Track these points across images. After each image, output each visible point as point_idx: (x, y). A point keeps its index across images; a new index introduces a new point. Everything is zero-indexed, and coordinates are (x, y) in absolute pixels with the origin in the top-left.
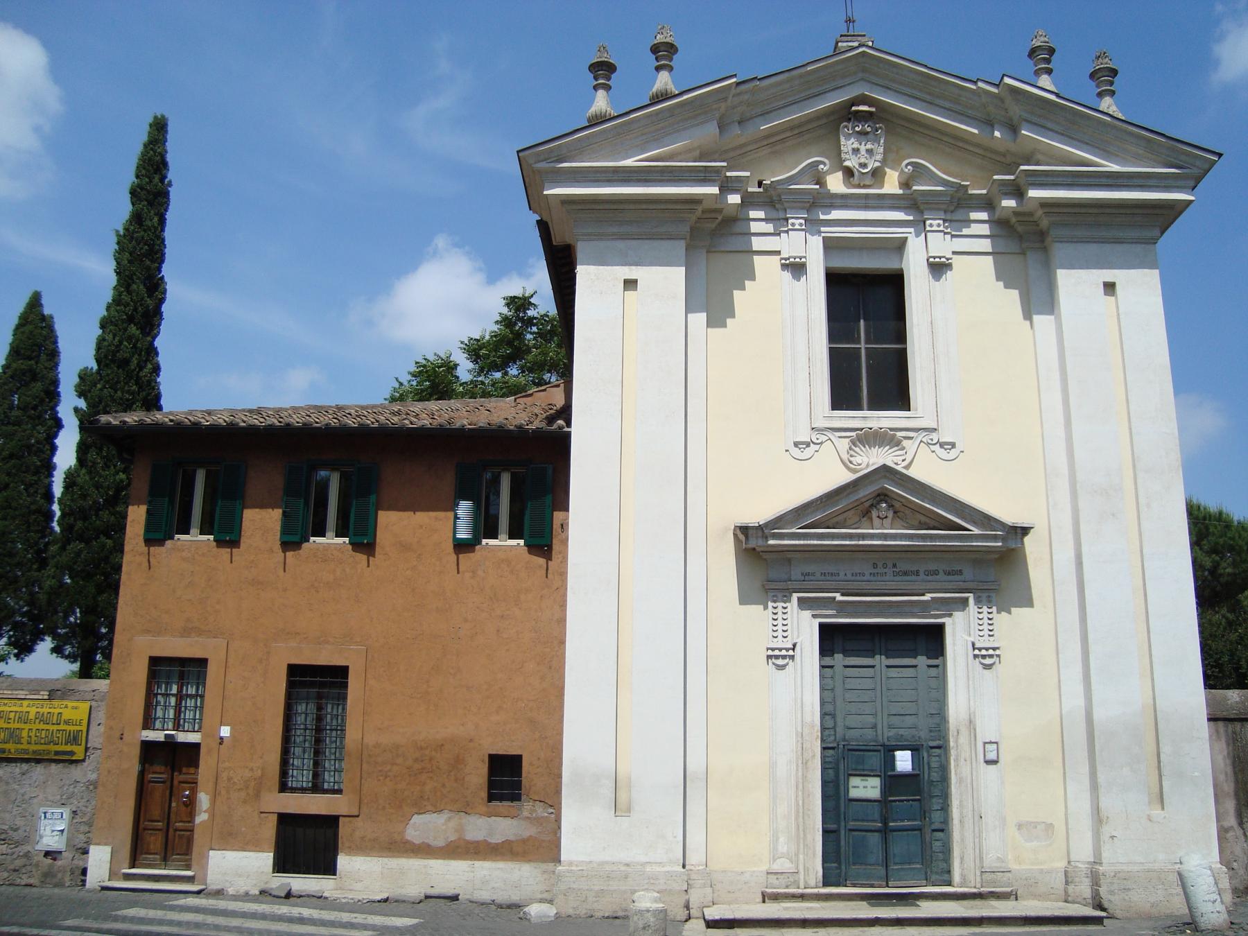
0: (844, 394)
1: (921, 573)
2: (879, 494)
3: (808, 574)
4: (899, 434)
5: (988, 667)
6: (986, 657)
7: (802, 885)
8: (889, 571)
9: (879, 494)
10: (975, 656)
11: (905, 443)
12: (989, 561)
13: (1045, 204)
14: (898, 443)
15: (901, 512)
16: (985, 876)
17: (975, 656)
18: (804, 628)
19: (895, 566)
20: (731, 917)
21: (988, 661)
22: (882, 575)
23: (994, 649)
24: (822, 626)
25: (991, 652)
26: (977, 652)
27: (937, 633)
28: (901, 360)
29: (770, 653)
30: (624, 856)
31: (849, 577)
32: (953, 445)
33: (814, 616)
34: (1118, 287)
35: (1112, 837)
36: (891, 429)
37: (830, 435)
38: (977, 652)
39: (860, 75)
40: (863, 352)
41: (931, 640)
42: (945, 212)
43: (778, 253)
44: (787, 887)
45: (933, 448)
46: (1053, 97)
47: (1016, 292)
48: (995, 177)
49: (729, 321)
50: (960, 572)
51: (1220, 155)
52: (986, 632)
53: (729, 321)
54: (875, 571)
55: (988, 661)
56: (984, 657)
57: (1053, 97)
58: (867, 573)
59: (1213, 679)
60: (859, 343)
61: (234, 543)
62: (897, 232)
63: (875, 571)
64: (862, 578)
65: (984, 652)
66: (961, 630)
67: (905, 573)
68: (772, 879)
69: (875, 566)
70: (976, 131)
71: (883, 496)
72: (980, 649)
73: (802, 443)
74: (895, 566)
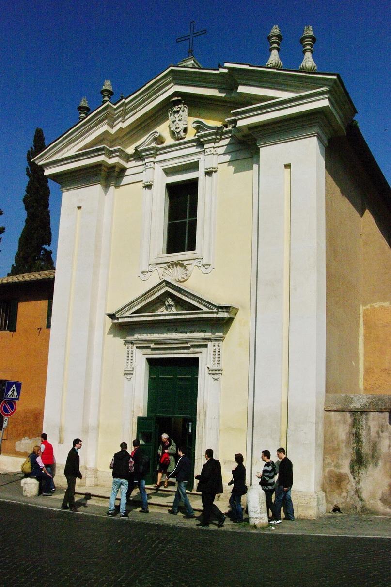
2: (171, 295)
4: (185, 263)
6: (215, 373)
9: (171, 295)
25: (217, 372)
26: (211, 372)
36: (181, 261)
37: (155, 266)
38: (211, 372)
40: (185, 220)
43: (142, 181)
45: (200, 268)
46: (275, 71)
47: (63, 194)
48: (226, 120)
52: (216, 362)
55: (216, 377)
56: (213, 374)
57: (275, 71)
60: (186, 218)
61: (14, 331)
65: (214, 372)
66: (206, 359)
72: (212, 371)
73: (145, 272)
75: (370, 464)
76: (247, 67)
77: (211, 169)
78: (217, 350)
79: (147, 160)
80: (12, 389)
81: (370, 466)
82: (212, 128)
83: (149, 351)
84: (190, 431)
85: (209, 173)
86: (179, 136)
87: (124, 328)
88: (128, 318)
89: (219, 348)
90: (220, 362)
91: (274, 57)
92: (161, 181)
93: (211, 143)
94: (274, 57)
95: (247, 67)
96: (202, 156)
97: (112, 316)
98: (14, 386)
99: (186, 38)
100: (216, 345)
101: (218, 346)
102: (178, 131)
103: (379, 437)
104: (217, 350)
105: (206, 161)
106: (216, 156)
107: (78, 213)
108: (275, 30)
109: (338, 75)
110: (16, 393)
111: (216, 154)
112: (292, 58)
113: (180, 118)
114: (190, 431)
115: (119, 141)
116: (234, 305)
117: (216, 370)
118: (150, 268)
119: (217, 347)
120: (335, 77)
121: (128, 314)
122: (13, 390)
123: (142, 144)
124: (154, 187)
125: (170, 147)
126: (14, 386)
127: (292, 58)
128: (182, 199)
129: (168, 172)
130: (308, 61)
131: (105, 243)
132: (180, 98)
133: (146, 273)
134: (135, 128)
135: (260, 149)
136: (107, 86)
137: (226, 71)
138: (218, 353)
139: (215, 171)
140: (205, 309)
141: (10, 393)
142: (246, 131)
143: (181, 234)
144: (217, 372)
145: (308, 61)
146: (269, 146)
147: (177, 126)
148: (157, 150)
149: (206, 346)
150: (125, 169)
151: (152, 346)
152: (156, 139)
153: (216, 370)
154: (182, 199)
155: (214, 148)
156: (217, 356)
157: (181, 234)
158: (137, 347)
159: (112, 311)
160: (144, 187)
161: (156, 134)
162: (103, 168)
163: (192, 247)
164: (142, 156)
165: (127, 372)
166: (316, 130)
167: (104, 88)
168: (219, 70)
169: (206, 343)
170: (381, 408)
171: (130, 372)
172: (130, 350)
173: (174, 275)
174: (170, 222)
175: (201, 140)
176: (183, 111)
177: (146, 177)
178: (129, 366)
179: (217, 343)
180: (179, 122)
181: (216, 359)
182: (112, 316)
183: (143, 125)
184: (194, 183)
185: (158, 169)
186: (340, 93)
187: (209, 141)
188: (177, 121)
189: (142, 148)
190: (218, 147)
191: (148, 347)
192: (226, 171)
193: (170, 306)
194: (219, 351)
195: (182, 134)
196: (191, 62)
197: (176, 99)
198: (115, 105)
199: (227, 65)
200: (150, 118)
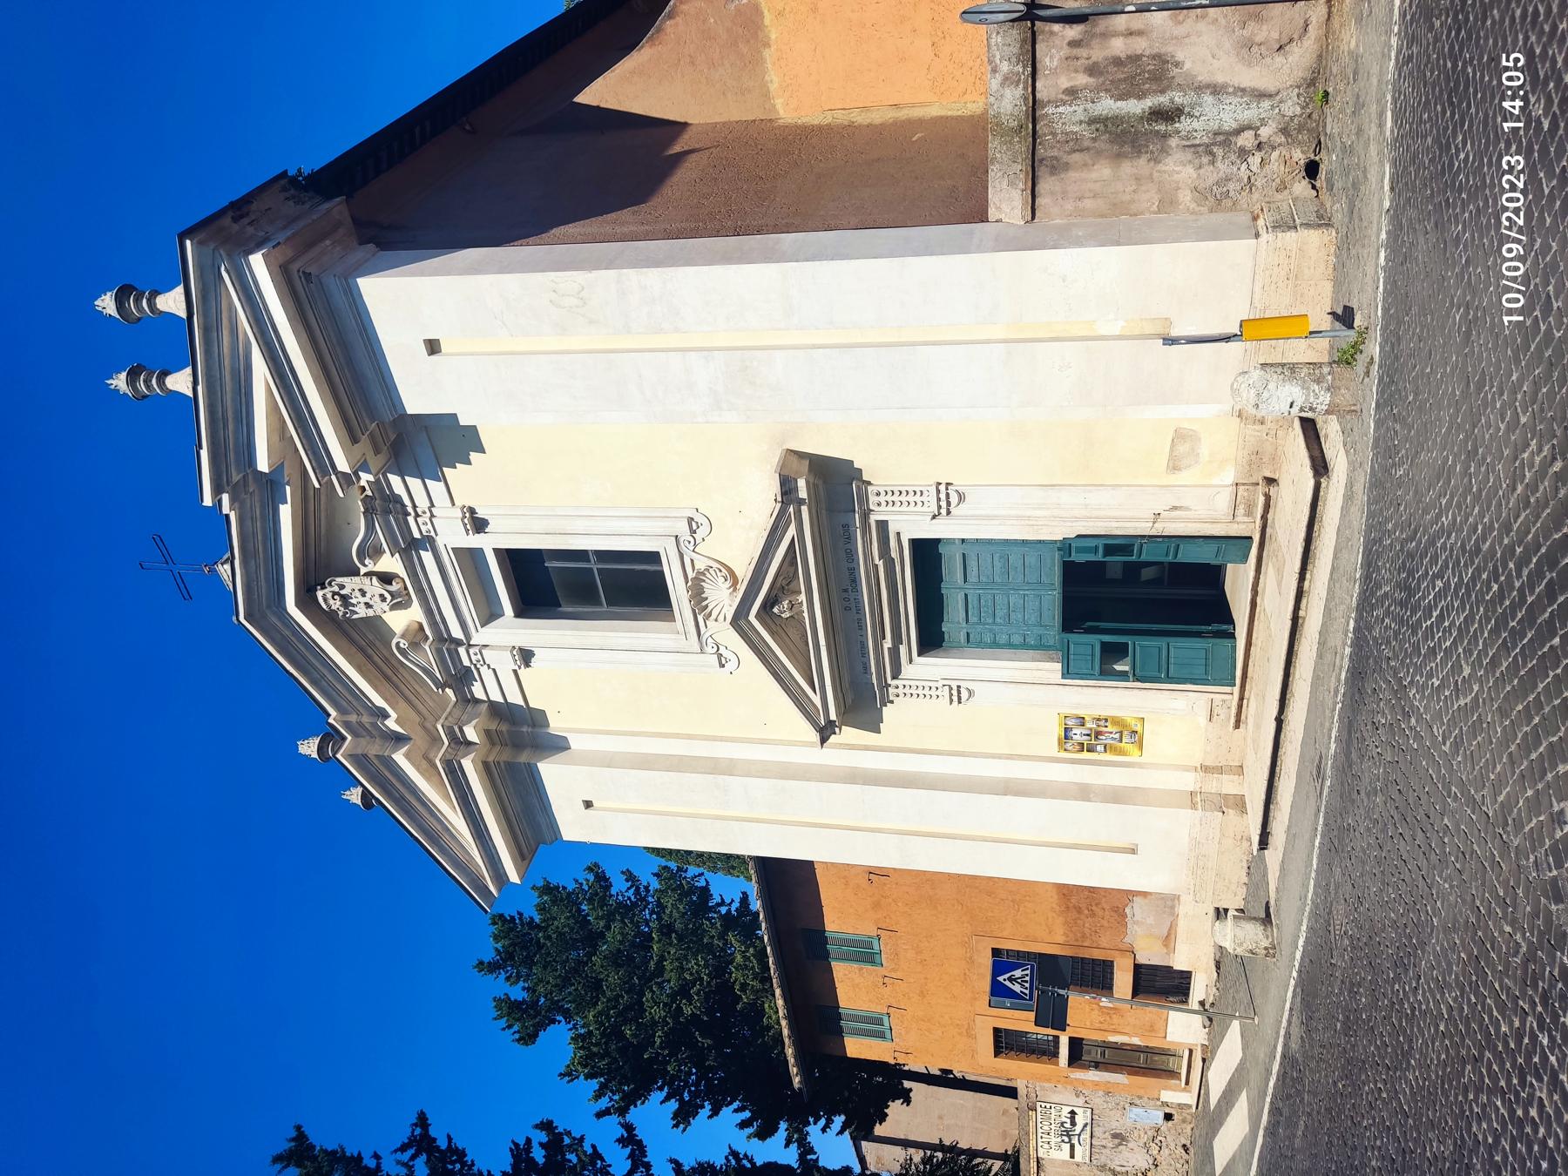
2: (766, 609)
4: (691, 575)
5: (961, 497)
9: (766, 609)
10: (949, 513)
12: (826, 492)
13: (351, 435)
15: (784, 586)
17: (949, 513)
18: (922, 669)
19: (846, 591)
24: (920, 655)
25: (943, 496)
26: (944, 511)
27: (917, 544)
30: (766, 12)
32: (690, 520)
38: (944, 511)
41: (926, 553)
43: (515, 672)
49: (473, 456)
52: (918, 498)
53: (473, 456)
56: (949, 504)
65: (943, 504)
66: (911, 525)
70: (288, 488)
72: (940, 507)
76: (204, 454)
78: (889, 498)
79: (466, 662)
80: (1007, 983)
82: (370, 528)
83: (903, 649)
85: (479, 525)
87: (859, 701)
91: (180, 382)
92: (510, 631)
94: (180, 382)
95: (204, 454)
96: (440, 542)
97: (825, 732)
98: (1001, 979)
100: (877, 499)
105: (452, 534)
106: (440, 505)
107: (607, 806)
108: (120, 382)
109: (182, 237)
110: (1018, 973)
112: (174, 344)
113: (358, 594)
115: (428, 725)
116: (775, 459)
117: (939, 499)
118: (709, 649)
119: (882, 499)
120: (188, 243)
121: (817, 700)
122: (1010, 979)
124: (526, 644)
125: (429, 612)
126: (1001, 979)
127: (174, 344)
128: (546, 583)
130: (172, 302)
131: (666, 752)
134: (397, 687)
136: (309, 748)
137: (225, 498)
139: (472, 511)
140: (792, 531)
141: (1017, 988)
142: (364, 445)
143: (625, 586)
144: (943, 496)
145: (172, 302)
149: (883, 526)
152: (415, 645)
153: (939, 499)
154: (546, 583)
155: (417, 515)
157: (625, 586)
158: (894, 677)
159: (814, 736)
160: (527, 665)
162: (491, 759)
163: (654, 557)
165: (955, 698)
166: (333, 284)
167: (315, 755)
168: (227, 516)
171: (955, 692)
173: (723, 599)
176: (342, 587)
177: (504, 663)
182: (825, 732)
183: (389, 672)
186: (231, 226)
188: (366, 599)
191: (895, 652)
192: (466, 482)
193: (792, 607)
195: (395, 587)
196: (224, 570)
198: (344, 739)
199: (208, 501)
200: (369, 657)
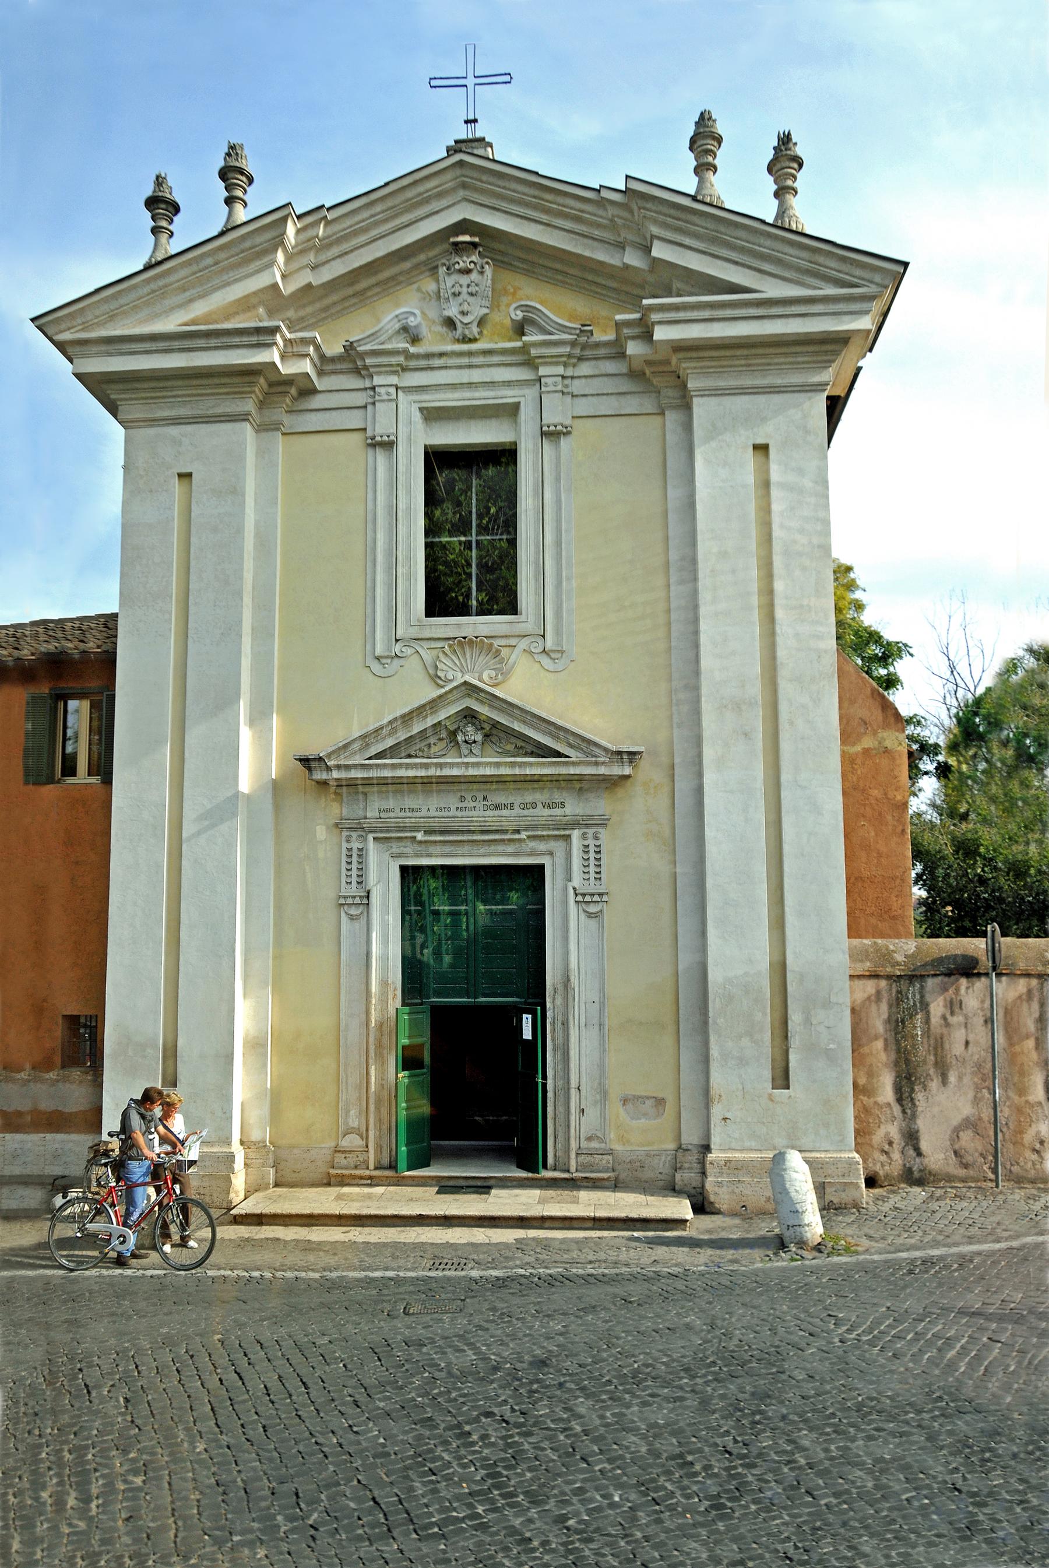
0: (441, 601)
1: (516, 806)
3: (386, 811)
4: (496, 643)
7: (371, 1166)
8: (480, 805)
11: (504, 652)
14: (498, 653)
15: (494, 734)
16: (581, 1158)
19: (485, 798)
20: (259, 1212)
21: (592, 909)
22: (470, 809)
23: (600, 895)
25: (596, 898)
28: (508, 558)
29: (342, 901)
31: (433, 813)
33: (393, 856)
34: (772, 450)
35: (725, 1119)
38: (579, 898)
39: (462, 193)
42: (565, 365)
44: (356, 1167)
50: (562, 805)
51: (906, 265)
52: (592, 875)
54: (463, 805)
55: (592, 909)
58: (454, 808)
59: (853, 931)
62: (509, 396)
63: (463, 805)
64: (446, 814)
65: (588, 898)
67: (497, 807)
68: (340, 1159)
69: (462, 799)
71: (469, 716)
72: (584, 895)
74: (485, 798)
75: (932, 1080)
77: (559, 428)
78: (592, 849)
79: (377, 380)
81: (934, 1085)
83: (409, 849)
84: (527, 1035)
86: (467, 332)
88: (357, 765)
89: (598, 843)
90: (603, 876)
93: (557, 364)
99: (456, 83)
101: (596, 838)
102: (466, 320)
103: (947, 1025)
104: (592, 849)
111: (568, 393)
114: (527, 1035)
119: (591, 842)
121: (358, 760)
123: (368, 337)
129: (432, 415)
132: (477, 240)
133: (389, 661)
135: (695, 400)
138: (595, 855)
146: (715, 395)
147: (465, 307)
148: (409, 356)
150: (314, 391)
151: (420, 836)
155: (563, 377)
156: (592, 862)
159: (311, 752)
161: (412, 319)
164: (366, 367)
169: (567, 832)
170: (948, 968)
172: (356, 845)
174: (429, 540)
175: (533, 352)
178: (354, 884)
179: (590, 832)
180: (470, 299)
181: (592, 869)
184: (504, 457)
185: (409, 407)
187: (554, 360)
188: (464, 296)
189: (368, 347)
190: (572, 378)
194: (597, 850)
197: (466, 238)
